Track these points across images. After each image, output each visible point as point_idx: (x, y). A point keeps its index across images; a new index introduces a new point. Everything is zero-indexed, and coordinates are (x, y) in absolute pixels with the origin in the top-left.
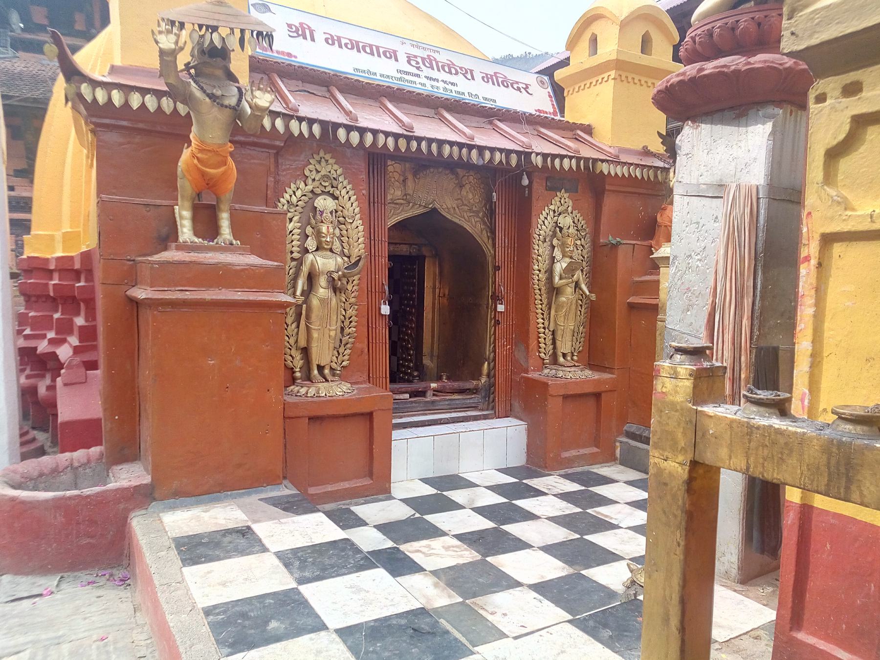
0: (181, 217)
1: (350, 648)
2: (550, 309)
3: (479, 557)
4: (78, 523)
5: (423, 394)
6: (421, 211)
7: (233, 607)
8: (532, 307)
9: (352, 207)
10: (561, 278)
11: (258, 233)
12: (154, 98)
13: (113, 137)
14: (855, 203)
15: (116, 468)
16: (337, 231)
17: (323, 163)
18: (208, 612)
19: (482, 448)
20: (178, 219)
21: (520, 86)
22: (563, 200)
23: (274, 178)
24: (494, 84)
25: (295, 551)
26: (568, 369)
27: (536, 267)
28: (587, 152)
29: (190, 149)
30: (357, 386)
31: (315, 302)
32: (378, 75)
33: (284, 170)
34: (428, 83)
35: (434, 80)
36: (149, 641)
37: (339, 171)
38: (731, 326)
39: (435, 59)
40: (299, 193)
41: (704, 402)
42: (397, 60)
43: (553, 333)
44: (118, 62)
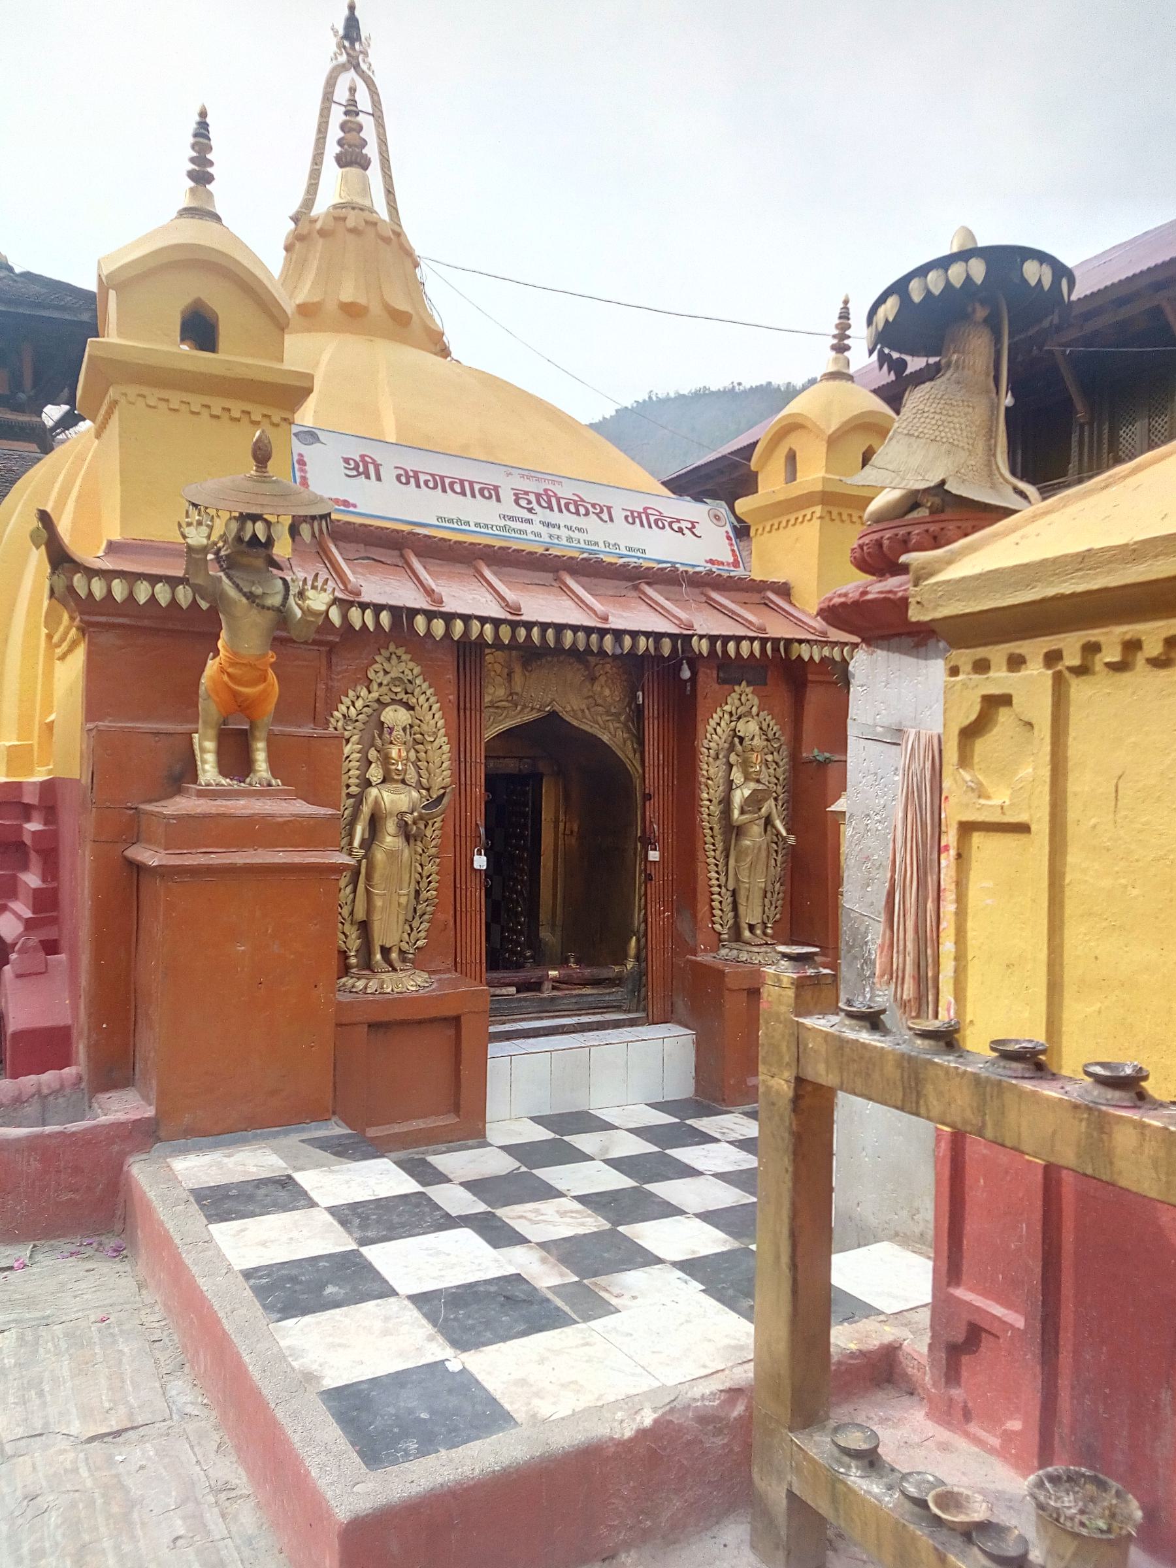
0: (203, 750)
1: (426, 1316)
2: (727, 856)
3: (608, 1226)
4: (59, 1172)
5: (536, 986)
6: (534, 715)
7: (279, 1270)
8: (700, 854)
9: (434, 719)
10: (742, 812)
11: (306, 768)
12: (167, 587)
13: (108, 639)
14: (991, 790)
15: (103, 1097)
16: (412, 754)
17: (394, 660)
18: (248, 1274)
19: (628, 1069)
20: (197, 752)
21: (683, 525)
22: (744, 696)
23: (326, 684)
24: (642, 525)
25: (354, 1206)
26: (756, 949)
27: (705, 795)
28: (779, 629)
29: (217, 659)
30: (437, 977)
31: (379, 856)
32: (472, 524)
33: (338, 674)
34: (544, 531)
35: (554, 526)
36: (163, 1323)
37: (417, 671)
38: (913, 910)
39: (555, 495)
40: (359, 704)
41: (808, 1013)
42: (498, 500)
43: (734, 893)
44: (116, 537)
